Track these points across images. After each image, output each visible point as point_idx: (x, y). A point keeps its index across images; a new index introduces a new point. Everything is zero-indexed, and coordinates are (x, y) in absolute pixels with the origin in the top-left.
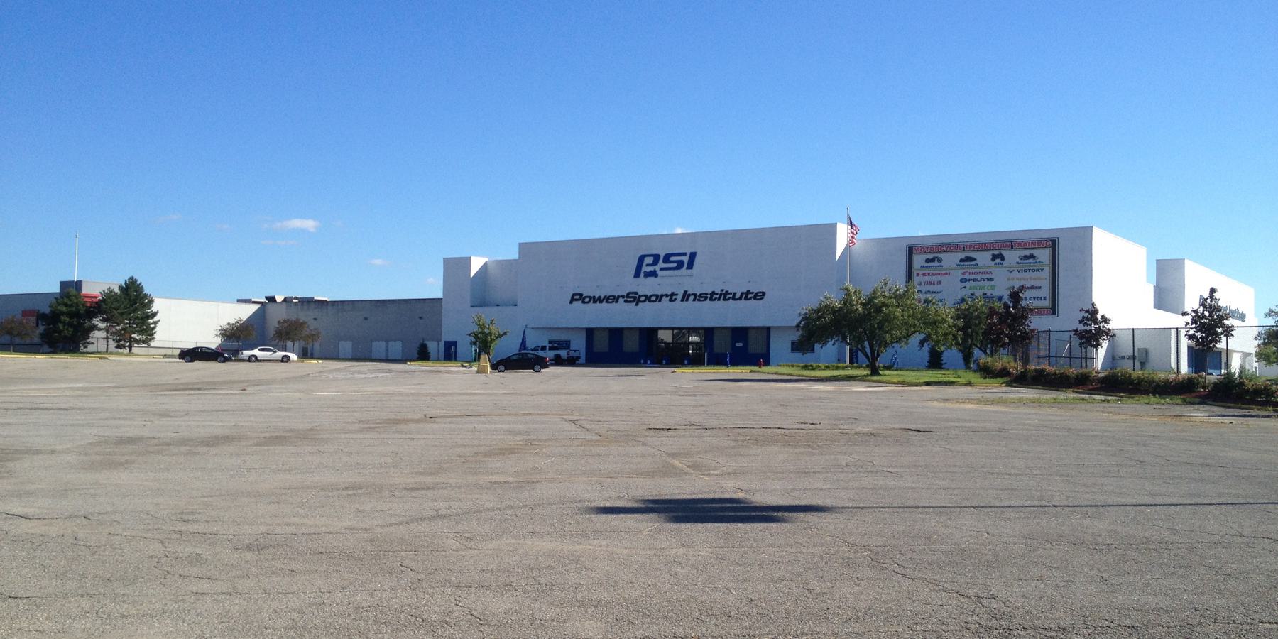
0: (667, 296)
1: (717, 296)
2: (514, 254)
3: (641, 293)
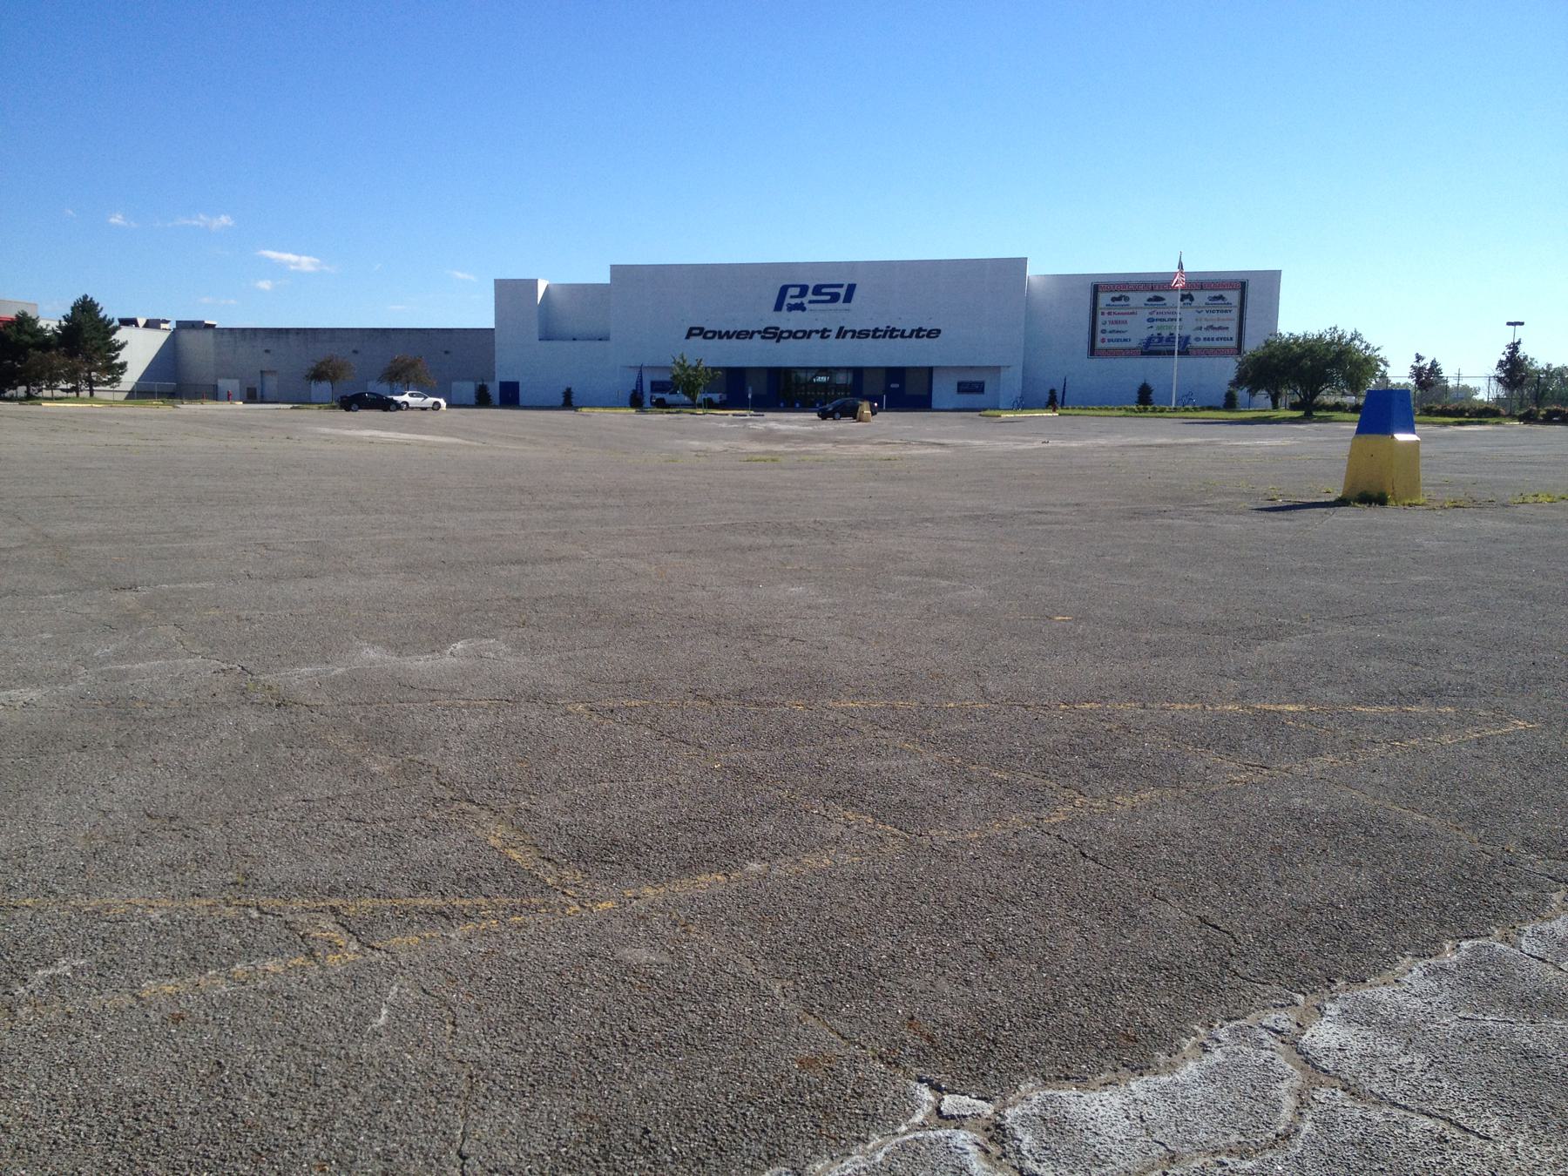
0: (817, 332)
1: (882, 333)
2: (605, 278)
3: (782, 328)
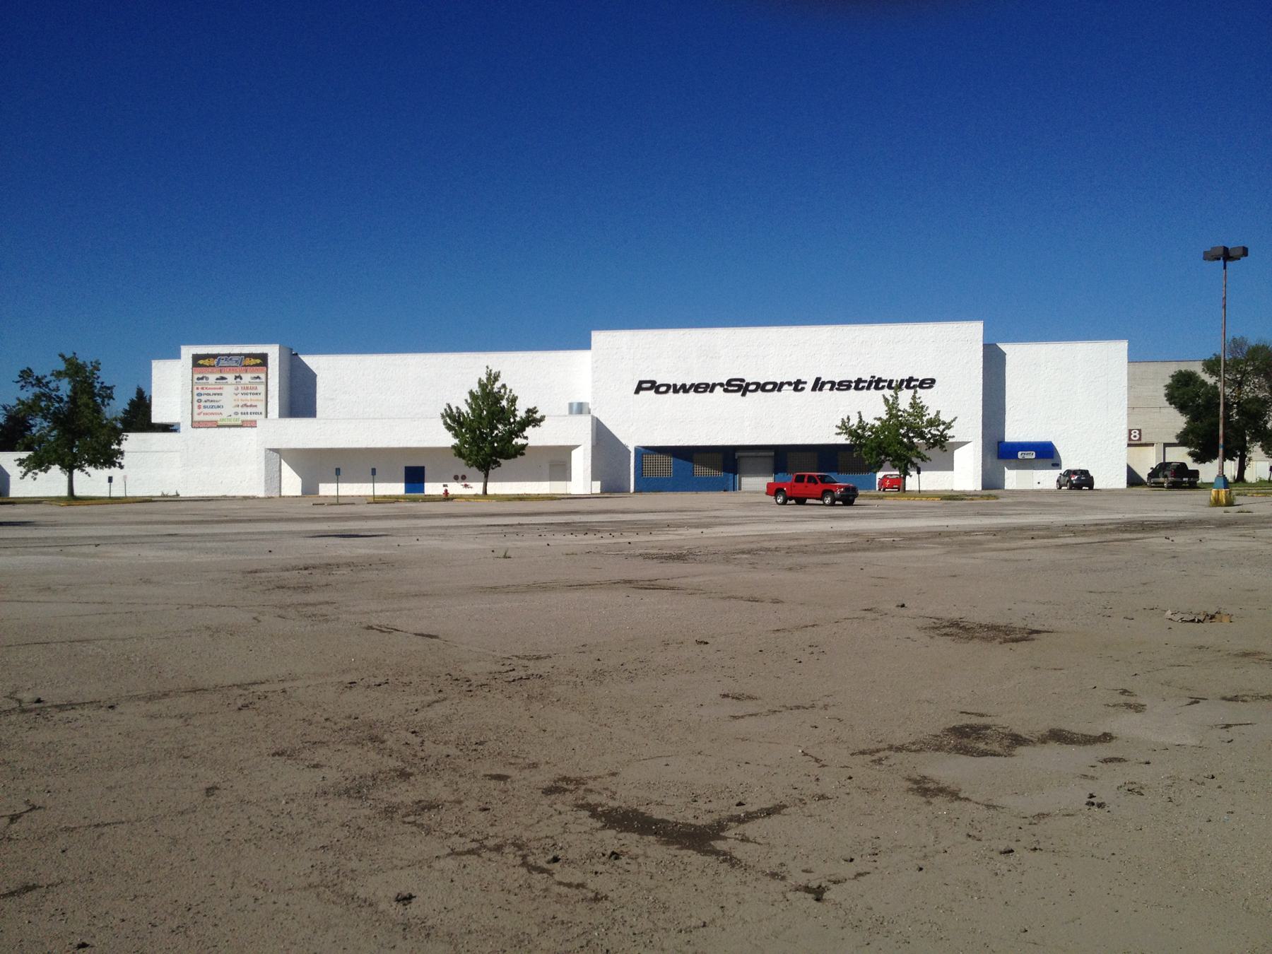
0: (789, 384)
